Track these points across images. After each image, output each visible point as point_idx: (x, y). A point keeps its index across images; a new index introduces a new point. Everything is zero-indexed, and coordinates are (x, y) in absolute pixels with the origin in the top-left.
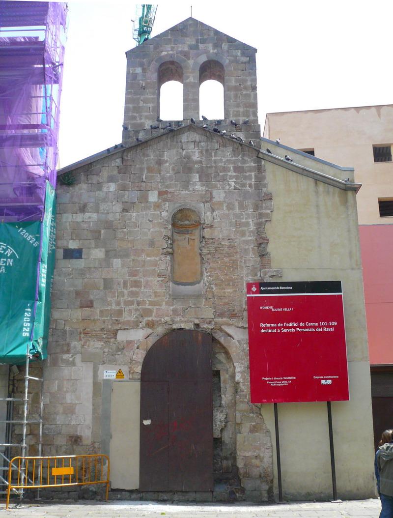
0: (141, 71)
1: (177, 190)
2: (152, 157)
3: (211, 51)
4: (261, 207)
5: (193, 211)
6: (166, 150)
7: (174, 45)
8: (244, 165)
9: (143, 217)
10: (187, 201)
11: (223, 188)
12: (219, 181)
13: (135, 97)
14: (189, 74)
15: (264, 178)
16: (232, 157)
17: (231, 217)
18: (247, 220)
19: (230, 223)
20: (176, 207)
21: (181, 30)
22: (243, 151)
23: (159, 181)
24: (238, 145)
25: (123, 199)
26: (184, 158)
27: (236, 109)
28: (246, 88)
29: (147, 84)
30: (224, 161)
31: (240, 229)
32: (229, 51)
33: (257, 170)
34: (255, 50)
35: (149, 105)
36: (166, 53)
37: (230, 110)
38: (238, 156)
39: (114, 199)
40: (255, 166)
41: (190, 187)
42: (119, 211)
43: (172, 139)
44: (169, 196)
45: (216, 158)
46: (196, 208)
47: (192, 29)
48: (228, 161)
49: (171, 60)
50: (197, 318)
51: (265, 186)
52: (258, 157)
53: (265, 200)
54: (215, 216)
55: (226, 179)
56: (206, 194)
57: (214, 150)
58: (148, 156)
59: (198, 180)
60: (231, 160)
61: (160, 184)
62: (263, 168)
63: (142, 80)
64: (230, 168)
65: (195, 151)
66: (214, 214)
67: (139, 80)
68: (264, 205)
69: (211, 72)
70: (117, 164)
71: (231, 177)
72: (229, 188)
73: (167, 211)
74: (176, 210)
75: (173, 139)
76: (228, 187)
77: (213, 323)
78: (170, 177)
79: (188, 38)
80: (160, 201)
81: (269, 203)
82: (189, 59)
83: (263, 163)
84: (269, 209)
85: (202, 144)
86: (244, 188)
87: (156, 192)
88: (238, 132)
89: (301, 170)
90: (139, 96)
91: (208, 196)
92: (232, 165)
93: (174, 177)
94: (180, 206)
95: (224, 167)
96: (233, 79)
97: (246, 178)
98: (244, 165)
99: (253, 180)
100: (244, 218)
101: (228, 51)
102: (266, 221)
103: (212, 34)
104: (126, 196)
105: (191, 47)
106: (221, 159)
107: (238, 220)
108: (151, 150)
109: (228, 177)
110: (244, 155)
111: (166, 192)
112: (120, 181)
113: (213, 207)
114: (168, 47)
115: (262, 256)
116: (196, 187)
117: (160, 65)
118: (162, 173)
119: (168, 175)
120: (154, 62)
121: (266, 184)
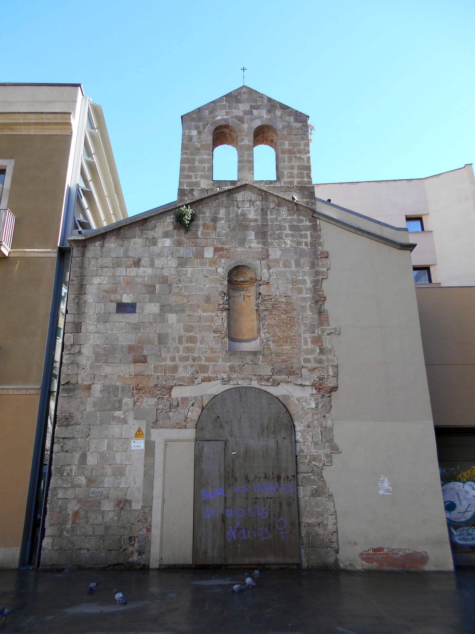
2: (208, 214)
3: (265, 117)
6: (221, 208)
11: (279, 245)
14: (242, 137)
15: (319, 237)
16: (288, 216)
17: (288, 275)
27: (290, 171)
28: (300, 152)
29: (202, 146)
31: (297, 286)
35: (204, 165)
41: (245, 244)
50: (255, 375)
51: (320, 244)
52: (313, 216)
55: (282, 237)
59: (254, 238)
60: (286, 219)
62: (318, 227)
66: (271, 271)
67: (195, 142)
69: (263, 136)
71: (287, 235)
72: (285, 246)
73: (223, 267)
76: (284, 245)
77: (271, 380)
80: (216, 257)
81: (325, 261)
82: (243, 123)
84: (325, 267)
86: (300, 247)
97: (301, 236)
99: (309, 239)
100: (301, 275)
101: (281, 117)
103: (266, 101)
105: (245, 113)
109: (284, 236)
111: (222, 249)
113: (269, 264)
115: (320, 313)
118: (218, 230)
121: (321, 242)
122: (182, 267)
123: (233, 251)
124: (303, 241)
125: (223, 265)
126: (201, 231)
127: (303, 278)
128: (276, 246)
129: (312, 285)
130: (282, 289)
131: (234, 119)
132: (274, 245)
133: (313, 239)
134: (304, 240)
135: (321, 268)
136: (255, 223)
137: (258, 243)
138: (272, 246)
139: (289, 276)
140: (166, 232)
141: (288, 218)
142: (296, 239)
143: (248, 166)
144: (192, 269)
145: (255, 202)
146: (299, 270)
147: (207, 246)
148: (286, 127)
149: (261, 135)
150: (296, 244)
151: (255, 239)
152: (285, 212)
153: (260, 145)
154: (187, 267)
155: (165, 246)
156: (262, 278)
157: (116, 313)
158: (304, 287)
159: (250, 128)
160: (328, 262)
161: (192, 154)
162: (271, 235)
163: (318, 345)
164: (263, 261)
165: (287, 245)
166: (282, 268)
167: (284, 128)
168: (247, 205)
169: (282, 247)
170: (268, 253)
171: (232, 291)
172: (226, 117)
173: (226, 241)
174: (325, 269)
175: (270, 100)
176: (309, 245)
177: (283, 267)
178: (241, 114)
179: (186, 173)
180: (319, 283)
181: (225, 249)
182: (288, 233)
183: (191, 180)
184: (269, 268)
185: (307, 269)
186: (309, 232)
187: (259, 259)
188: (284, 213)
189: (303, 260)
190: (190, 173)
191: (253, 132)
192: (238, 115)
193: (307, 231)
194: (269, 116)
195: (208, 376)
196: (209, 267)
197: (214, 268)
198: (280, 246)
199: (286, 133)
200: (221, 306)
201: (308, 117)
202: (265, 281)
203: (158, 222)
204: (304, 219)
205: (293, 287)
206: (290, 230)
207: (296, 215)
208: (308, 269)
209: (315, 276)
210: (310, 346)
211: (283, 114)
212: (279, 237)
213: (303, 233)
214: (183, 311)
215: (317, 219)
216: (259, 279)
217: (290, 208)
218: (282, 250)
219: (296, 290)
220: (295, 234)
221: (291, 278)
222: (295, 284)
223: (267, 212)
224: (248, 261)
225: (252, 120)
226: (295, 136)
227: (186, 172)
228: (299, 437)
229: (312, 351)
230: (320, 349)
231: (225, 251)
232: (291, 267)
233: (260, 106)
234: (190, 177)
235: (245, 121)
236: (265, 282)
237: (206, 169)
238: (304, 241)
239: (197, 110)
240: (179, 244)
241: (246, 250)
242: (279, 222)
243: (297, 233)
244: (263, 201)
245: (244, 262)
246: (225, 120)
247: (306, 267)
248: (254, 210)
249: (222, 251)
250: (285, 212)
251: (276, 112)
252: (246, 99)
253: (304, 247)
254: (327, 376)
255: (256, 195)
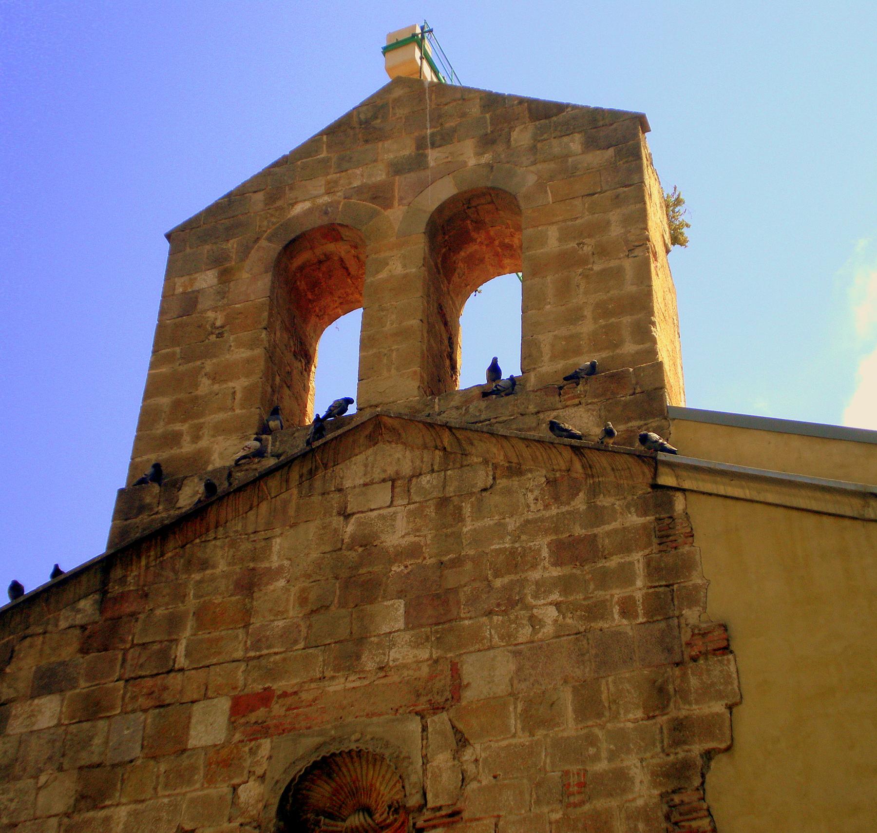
0: (215, 281)
1: (312, 681)
2: (222, 567)
3: (472, 162)
4: (683, 694)
5: (377, 759)
6: (278, 531)
7: (335, 176)
8: (596, 531)
9: (158, 820)
10: (350, 719)
11: (508, 637)
12: (489, 613)
13: (182, 368)
14: (383, 255)
15: (687, 565)
16: (547, 507)
17: (544, 758)
18: (617, 764)
19: (539, 785)
20: (301, 752)
21: (366, 124)
22: (593, 476)
23: (239, 654)
24: (567, 454)
25: (84, 754)
26: (351, 548)
27: (563, 331)
28: (602, 251)
29: (230, 320)
30: (510, 528)
31: (587, 807)
32: (539, 145)
33: (655, 541)
34: (639, 122)
35: (231, 384)
36: (307, 205)
37: (541, 337)
38: (574, 495)
39: (50, 758)
40: (644, 527)
41: (364, 658)
42: (59, 807)
43: (306, 484)
44: (277, 709)
45: (478, 524)
46: (387, 745)
47: (401, 112)
48: (529, 527)
49: (325, 221)
51: (692, 598)
52: (655, 486)
53: (694, 659)
54: (471, 769)
55: (521, 600)
56: (431, 677)
57: (472, 494)
58: (205, 565)
59: (401, 625)
60: (542, 520)
61: (243, 667)
62: (681, 529)
63: (215, 309)
64: (539, 550)
65: (394, 515)
66: (468, 755)
67: (206, 311)
68: (694, 682)
69: (491, 240)
70: (79, 616)
71: (542, 589)
72: (535, 631)
73: (262, 777)
74: (302, 766)
75: (311, 487)
76: (528, 630)
78: (288, 636)
79: (387, 144)
80: (238, 736)
81: (715, 668)
82: (388, 206)
83: (680, 503)
84: (720, 696)
85: (425, 480)
86: (601, 624)
87: (224, 704)
88: (572, 410)
89: (857, 502)
90: (199, 363)
91: (444, 681)
92: (548, 539)
93: (304, 631)
94: (318, 748)
95: (513, 552)
96: (553, 233)
97: (604, 579)
98: (596, 531)
99: (639, 583)
100: (604, 754)
101: (533, 149)
102: (708, 755)
103: (475, 110)
104: (97, 741)
105: (397, 169)
106: (500, 525)
107: (575, 768)
108: (218, 543)
109: (529, 591)
110: (594, 492)
111: (265, 698)
112: (83, 684)
113: (460, 726)
114: (317, 186)
116: (393, 654)
117: (286, 248)
118: (256, 622)
119: (281, 623)
120: (263, 243)
121: (696, 587)
122: (95, 807)
123: (311, 698)
124: (612, 596)
125: (265, 766)
126: (188, 639)
127: (613, 766)
128: (496, 639)
129: (656, 792)
132: (484, 638)
133: (659, 580)
134: (618, 591)
135: (697, 702)
136: (408, 563)
138: (477, 647)
139: (548, 768)
141: (547, 514)
142: (581, 596)
143: (398, 350)
144: (133, 807)
145: (414, 480)
146: (596, 731)
147: (206, 697)
148: (551, 179)
149: (480, 237)
150: (581, 618)
151: (407, 629)
153: (497, 279)
154: (112, 805)
155: (35, 728)
156: (429, 796)
158: (620, 808)
160: (733, 668)
161: (187, 358)
162: (473, 600)
164: (436, 718)
165: (542, 626)
166: (520, 733)
168: (383, 495)
169: (520, 640)
170: (460, 678)
173: (284, 660)
174: (718, 707)
176: (640, 611)
177: (523, 729)
178: (380, 175)
179: (160, 429)
180: (689, 778)
181: (279, 697)
182: (546, 575)
184: (462, 742)
186: (641, 553)
187: (417, 713)
188: (531, 497)
189: (614, 682)
190: (178, 427)
191: (422, 227)
192: (370, 182)
196: (202, 788)
197: (224, 789)
198: (509, 636)
199: (550, 200)
201: (639, 122)
202: (440, 808)
205: (566, 817)
207: (581, 494)
208: (636, 721)
209: (670, 746)
211: (542, 134)
212: (509, 599)
213: (614, 562)
215: (671, 493)
216: (414, 801)
217: (558, 475)
218: (517, 654)
219: (580, 825)
220: (579, 572)
221: (557, 774)
222: (576, 799)
223: (460, 508)
224: (369, 729)
226: (587, 199)
227: (162, 423)
231: (277, 706)
232: (558, 725)
233: (454, 130)
235: (393, 196)
236: (438, 814)
237: (239, 396)
238: (616, 599)
241: (366, 682)
244: (446, 470)
245: (353, 738)
247: (627, 711)
248: (410, 512)
249: (266, 706)
251: (515, 135)
252: (404, 120)
253: (617, 621)
255: (417, 453)
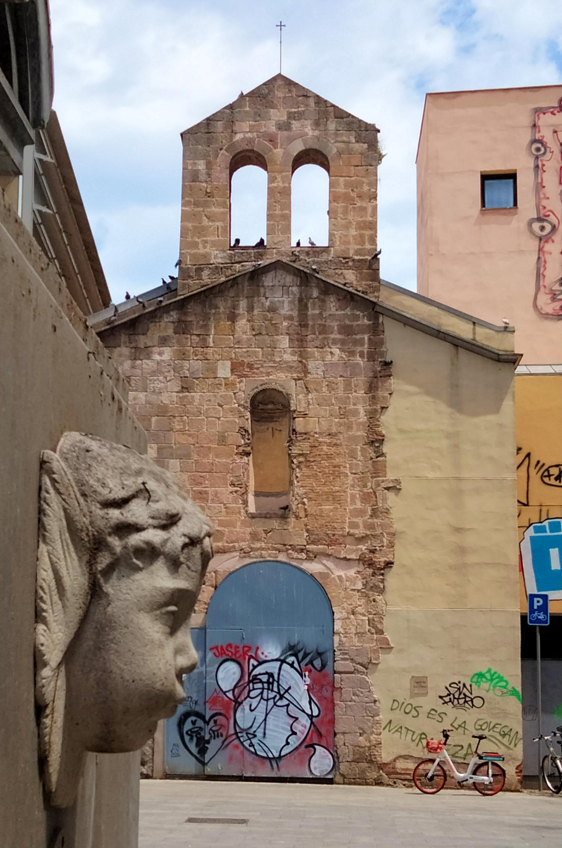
2: (222, 309)
3: (310, 133)
6: (241, 298)
16: (337, 310)
62: (381, 328)
66: (310, 396)
71: (335, 342)
99: (366, 346)
109: (330, 342)
121: (384, 351)
130: (325, 425)
131: (261, 140)
137: (293, 354)
140: (163, 337)
152: (334, 304)
157: (289, 644)
159: (286, 154)
161: (196, 204)
163: (371, 504)
167: (340, 153)
171: (257, 423)
172: (249, 135)
175: (319, 100)
178: (273, 129)
183: (196, 251)
185: (361, 393)
188: (332, 305)
193: (363, 333)
194: (317, 133)
195: (223, 546)
200: (241, 449)
203: (152, 322)
204: (361, 314)
206: (340, 333)
210: (359, 505)
213: (358, 337)
214: (188, 456)
225: (291, 140)
226: (356, 168)
228: (338, 626)
229: (361, 513)
230: (373, 510)
234: (195, 245)
238: (358, 351)
239: (205, 122)
240: (183, 356)
242: (324, 320)
243: (349, 337)
246: (250, 141)
250: (334, 304)
254: (379, 547)
